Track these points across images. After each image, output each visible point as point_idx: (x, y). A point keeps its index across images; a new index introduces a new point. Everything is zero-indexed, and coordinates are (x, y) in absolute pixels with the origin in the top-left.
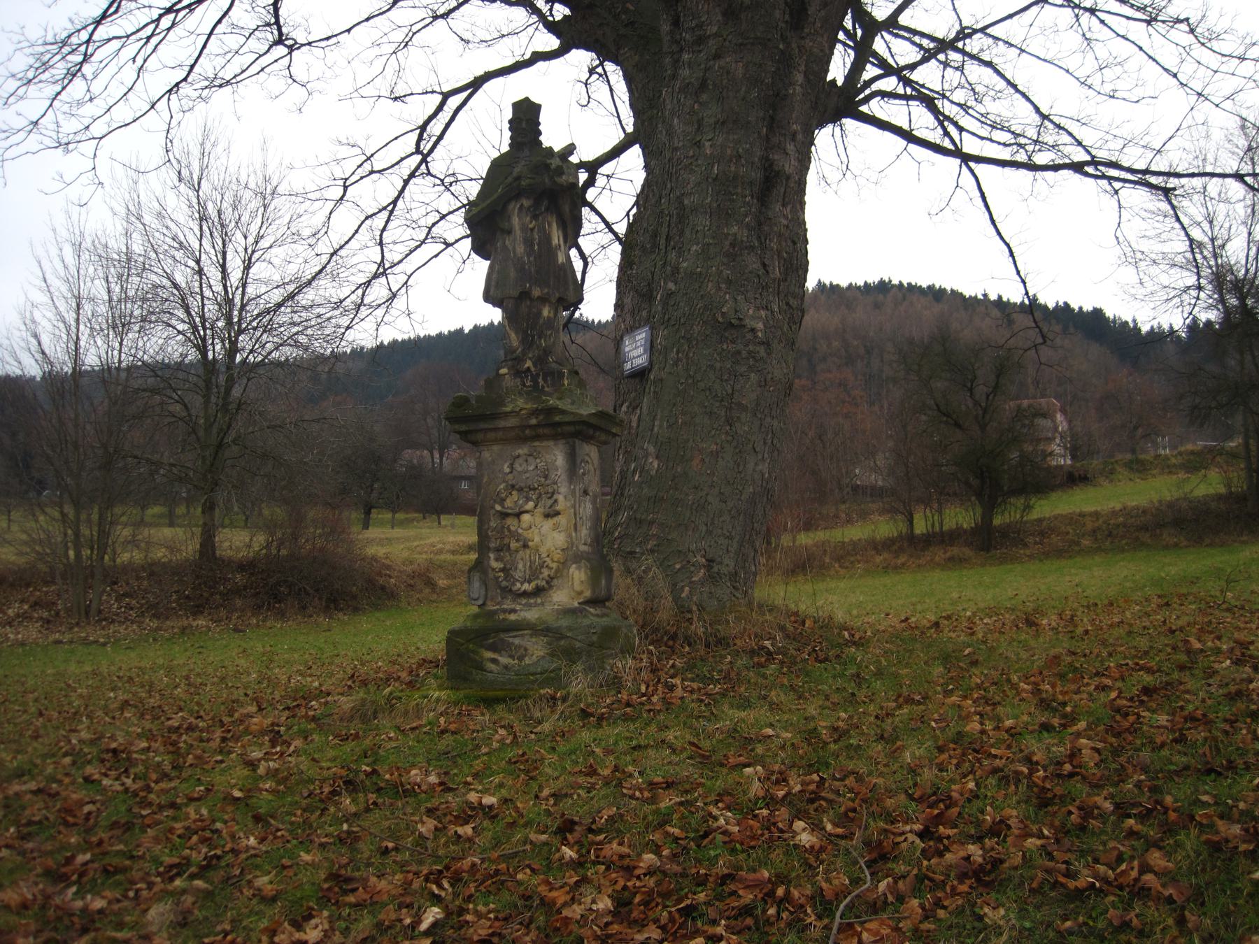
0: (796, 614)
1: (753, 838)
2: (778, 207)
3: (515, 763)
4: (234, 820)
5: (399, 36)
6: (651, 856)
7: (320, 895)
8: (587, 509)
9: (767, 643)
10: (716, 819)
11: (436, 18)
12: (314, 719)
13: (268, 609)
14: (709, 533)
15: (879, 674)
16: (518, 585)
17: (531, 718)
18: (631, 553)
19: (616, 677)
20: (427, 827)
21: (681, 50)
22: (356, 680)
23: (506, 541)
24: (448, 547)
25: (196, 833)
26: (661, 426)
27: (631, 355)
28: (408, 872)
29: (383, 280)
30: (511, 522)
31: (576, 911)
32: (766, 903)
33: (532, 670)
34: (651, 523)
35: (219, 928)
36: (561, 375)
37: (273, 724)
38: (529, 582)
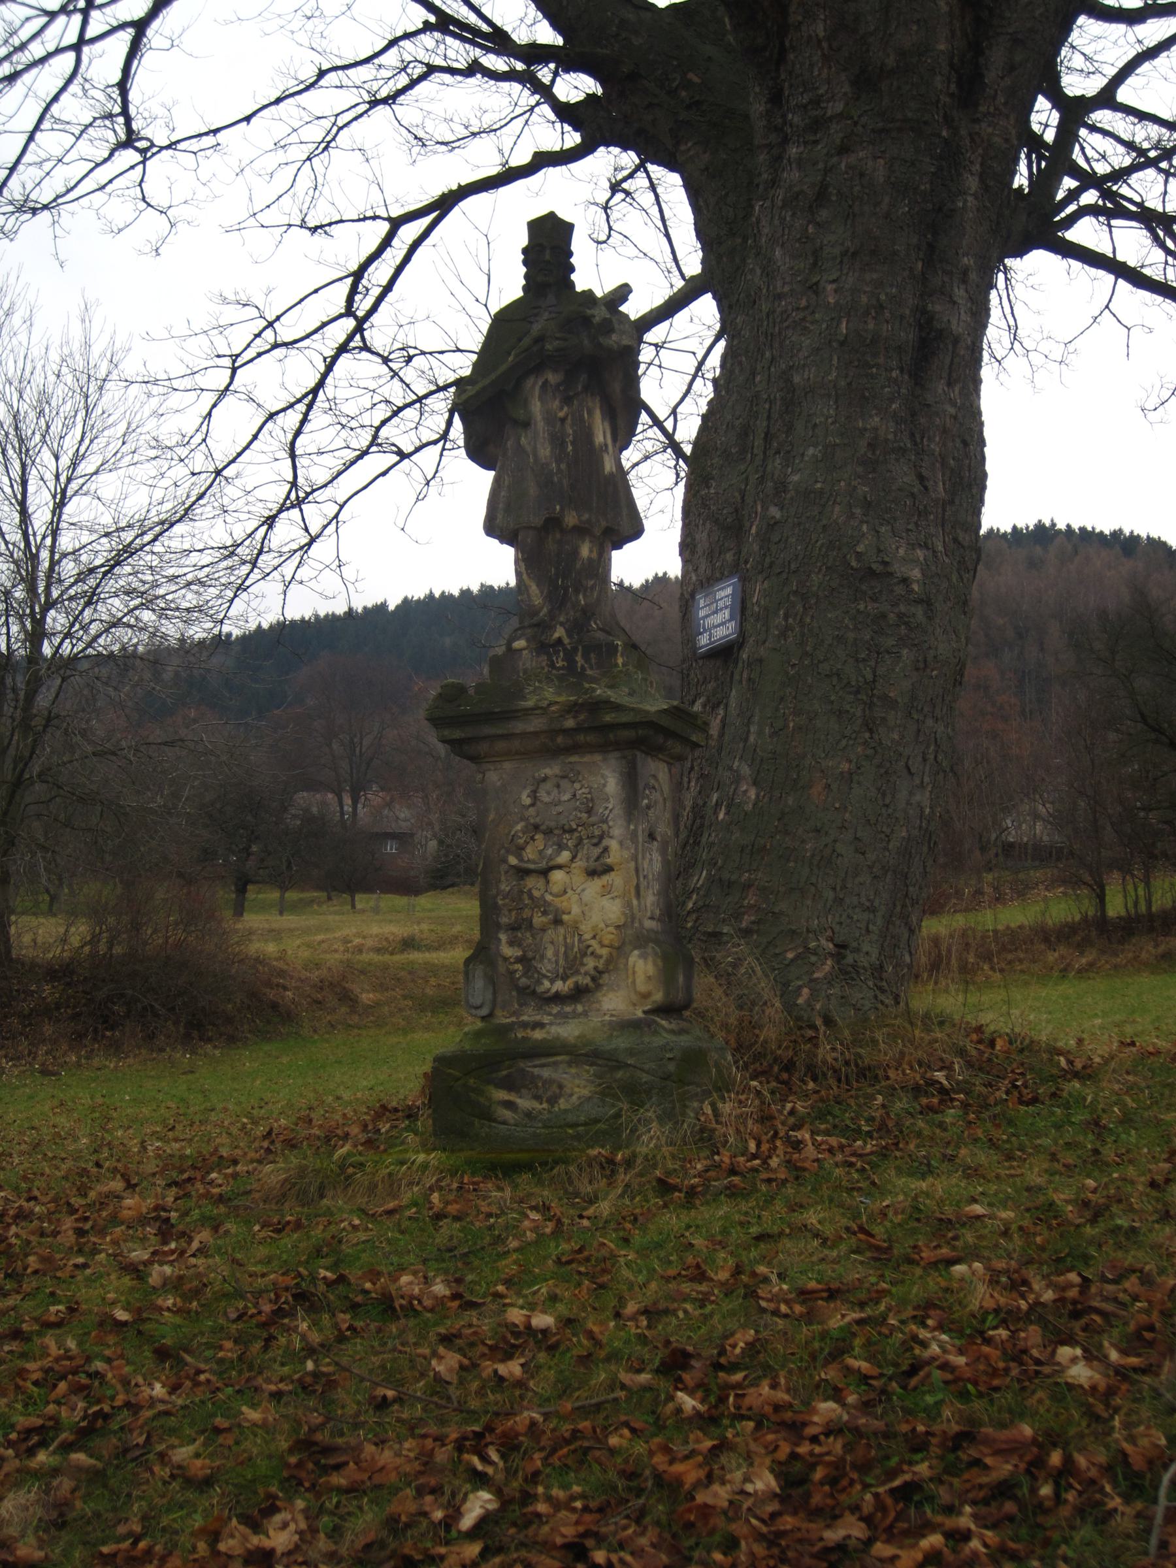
0: (979, 1029)
1: (995, 1373)
2: (941, 387)
3: (569, 1262)
4: (122, 1356)
5: (316, 133)
6: (830, 1405)
7: (285, 1474)
8: (654, 863)
9: (939, 1075)
10: (924, 1344)
11: (374, 103)
12: (221, 1199)
13: (95, 1039)
14: (839, 901)
15: (1127, 1120)
16: (547, 984)
17: (577, 1194)
18: (716, 935)
19: (702, 1130)
20: (446, 1364)
21: (786, 140)
22: (275, 1143)
23: (526, 913)
24: (369, 943)
25: (63, 1377)
26: (760, 733)
27: (711, 621)
28: (425, 1436)
29: (295, 513)
30: (533, 884)
31: (720, 1495)
32: (1034, 1478)
33: (571, 1118)
34: (748, 886)
35: (121, 1529)
36: (612, 650)
37: (157, 1208)
38: (564, 979)
